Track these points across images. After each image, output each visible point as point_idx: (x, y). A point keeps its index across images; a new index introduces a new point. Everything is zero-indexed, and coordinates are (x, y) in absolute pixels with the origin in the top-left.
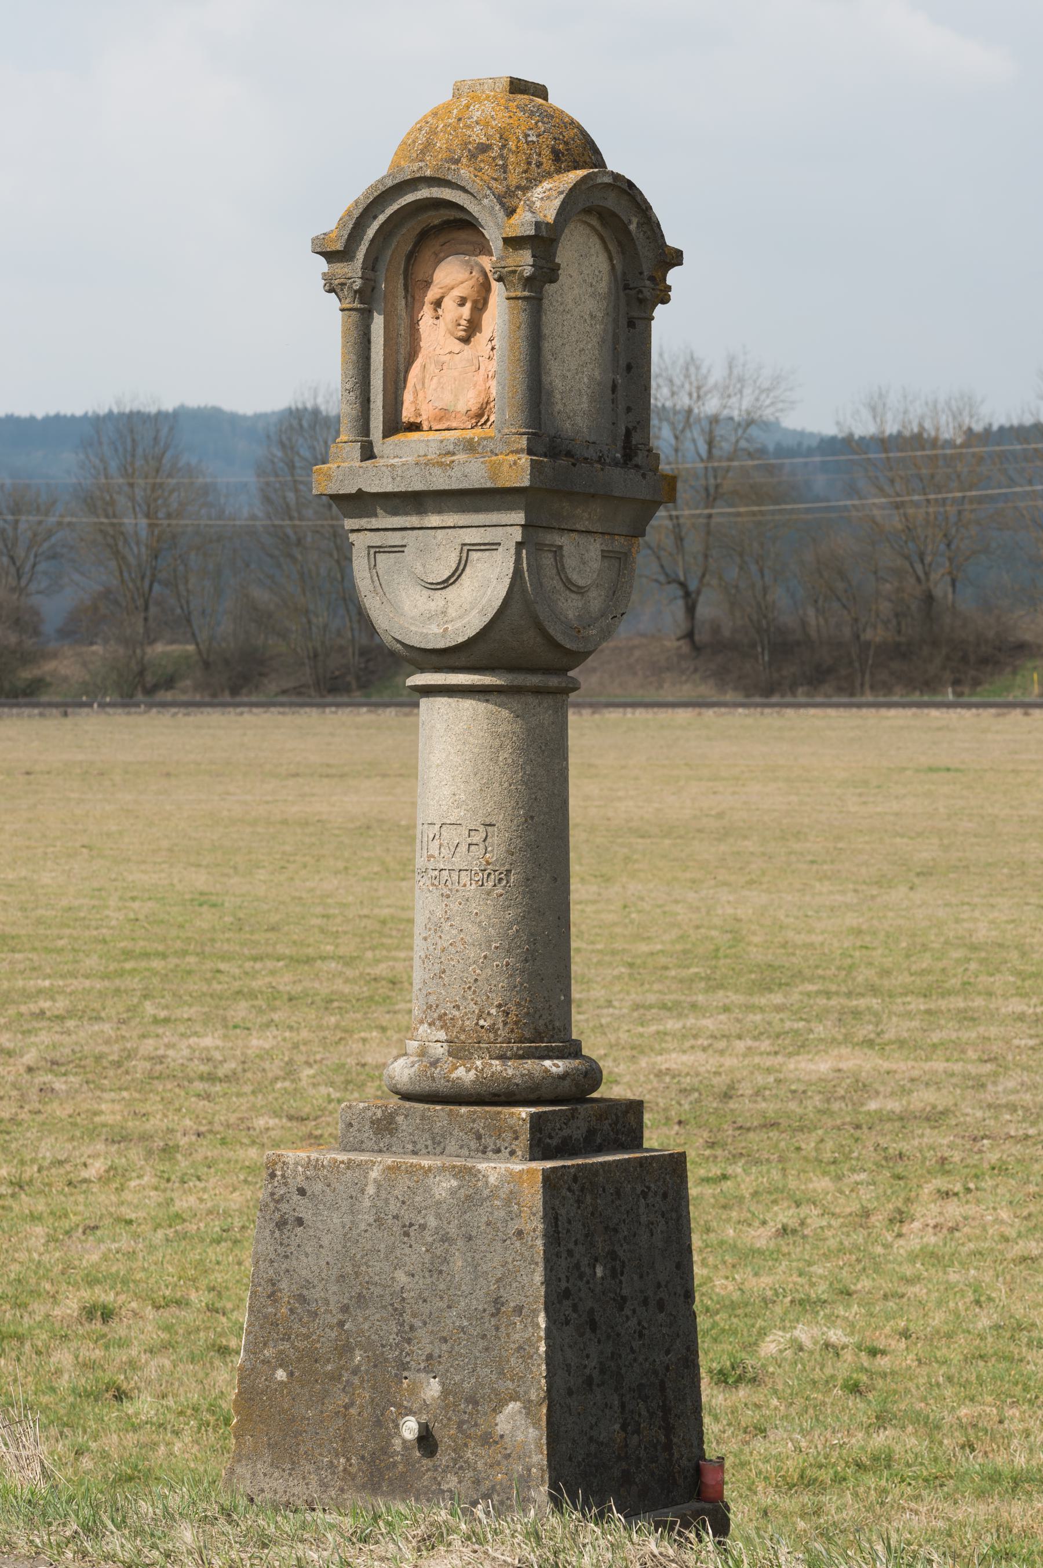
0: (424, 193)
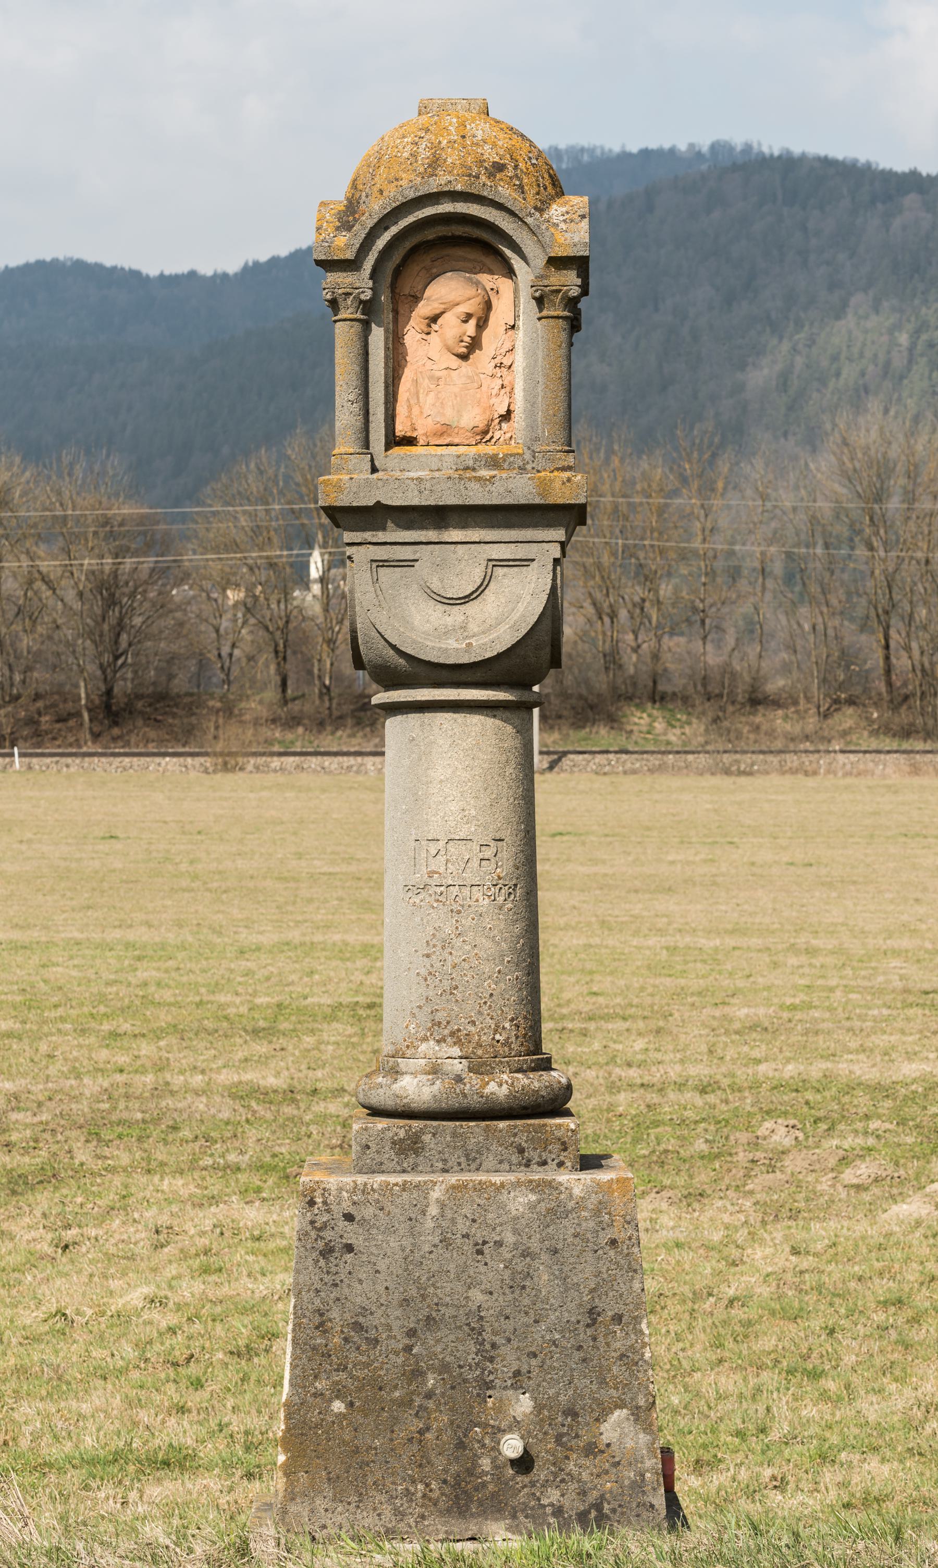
0: (446, 207)
